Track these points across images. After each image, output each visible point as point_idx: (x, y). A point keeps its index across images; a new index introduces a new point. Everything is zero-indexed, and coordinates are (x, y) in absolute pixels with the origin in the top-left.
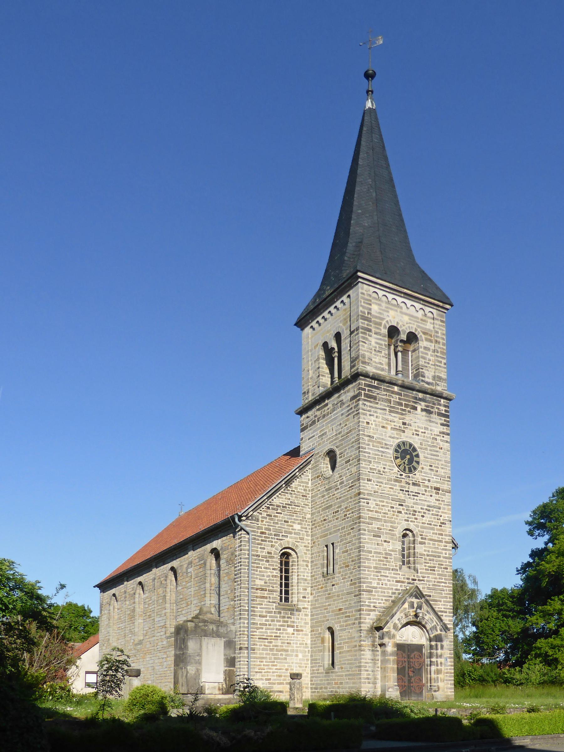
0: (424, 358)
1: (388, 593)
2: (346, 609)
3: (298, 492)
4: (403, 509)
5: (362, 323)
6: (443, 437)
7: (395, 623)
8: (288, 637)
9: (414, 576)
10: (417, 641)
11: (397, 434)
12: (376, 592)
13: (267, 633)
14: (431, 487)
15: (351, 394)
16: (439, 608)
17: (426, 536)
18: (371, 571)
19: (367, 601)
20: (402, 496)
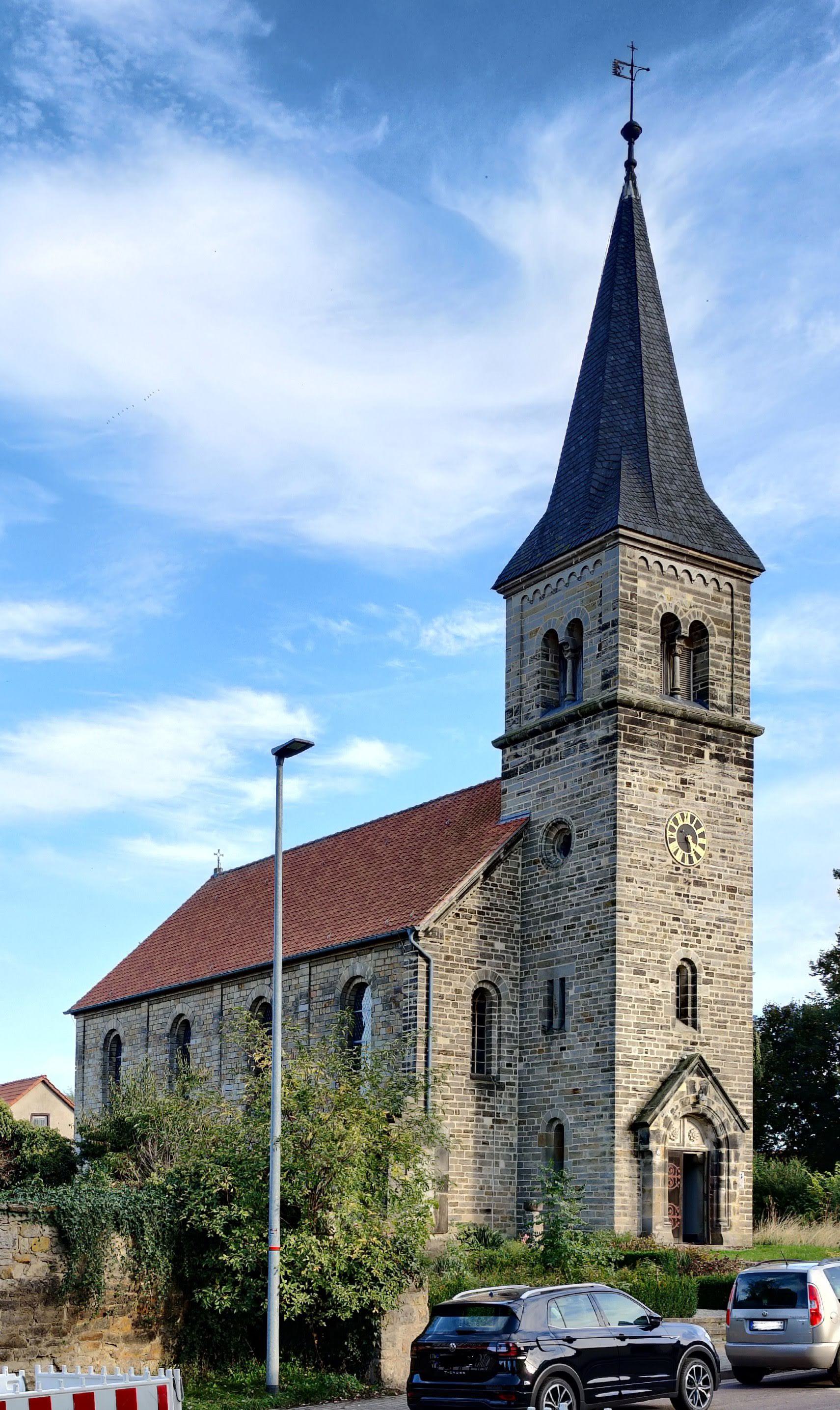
0: (716, 665)
2: (586, 1090)
3: (502, 886)
4: (680, 926)
5: (622, 614)
6: (743, 800)
8: (484, 1132)
9: (694, 1037)
11: (672, 800)
13: (453, 1125)
14: (723, 887)
15: (600, 733)
16: (731, 1090)
17: (714, 970)
19: (624, 1080)
20: (678, 904)
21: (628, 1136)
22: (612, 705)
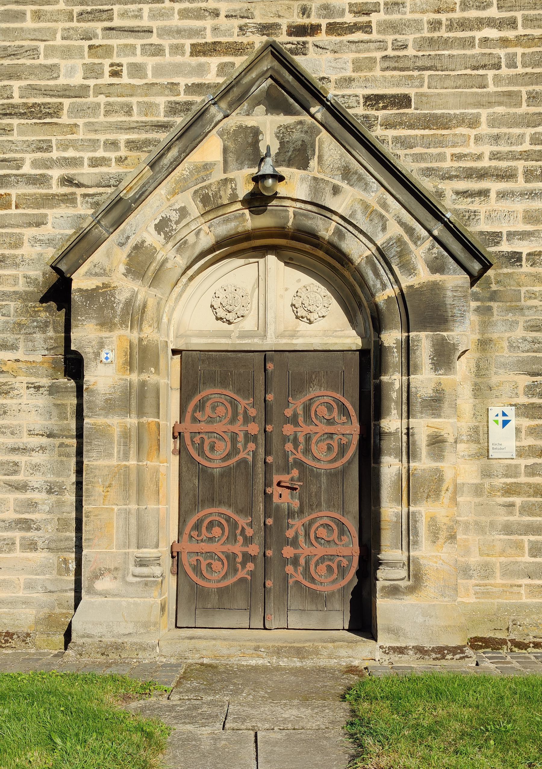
1: (148, 108)
10: (326, 333)
12: (76, 111)
18: (54, 18)
19: (29, 157)
21: (43, 315)
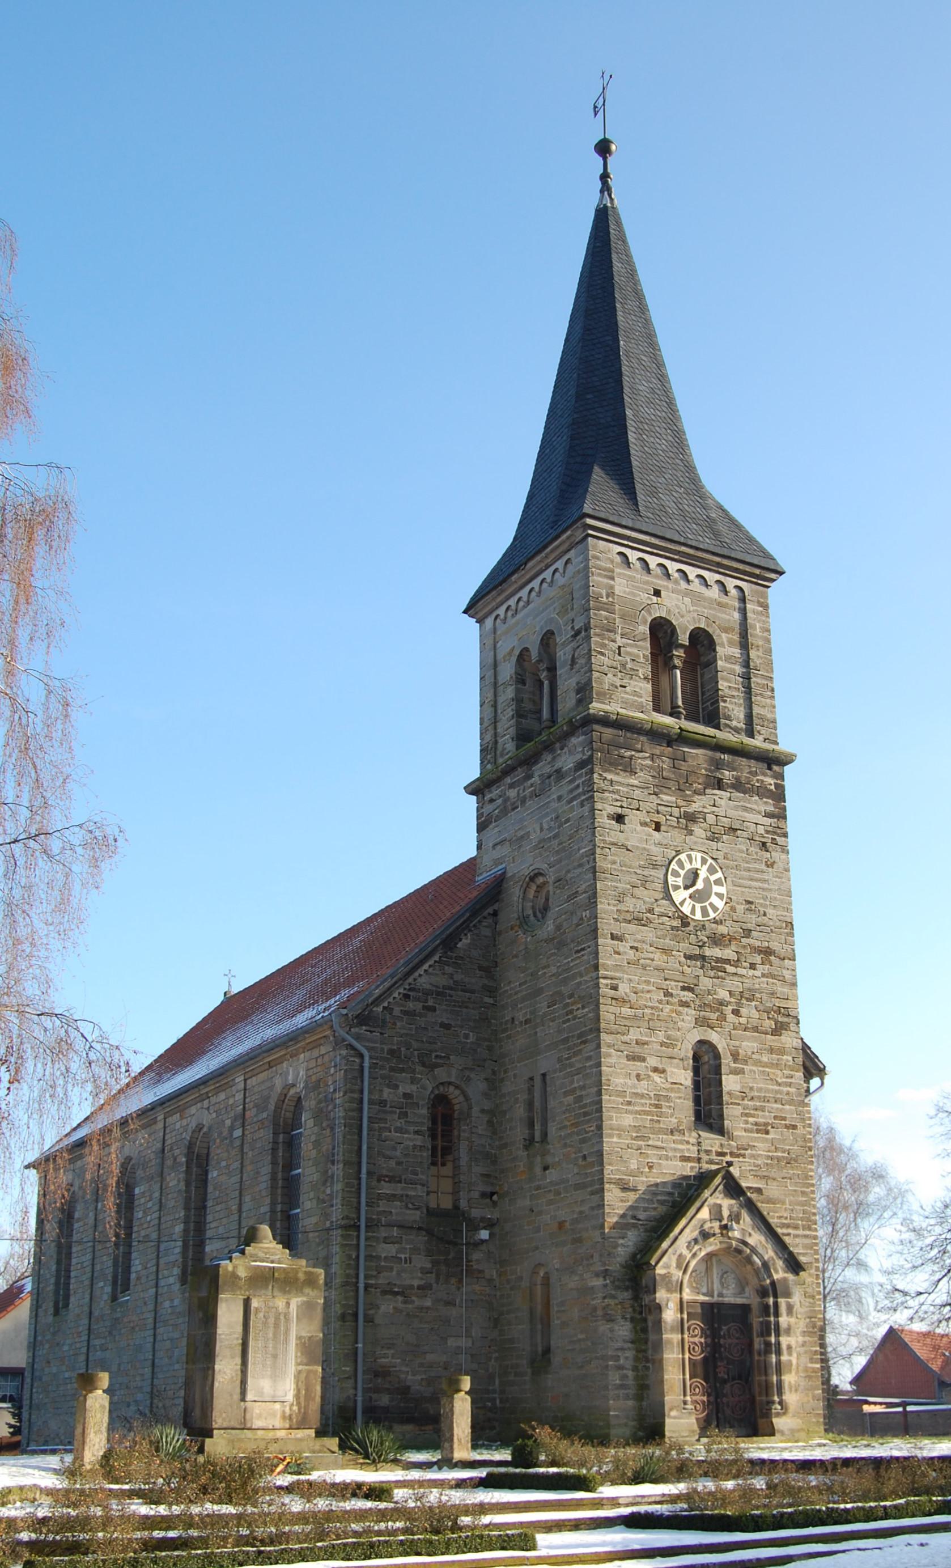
7: (680, 1255)
20: (692, 970)
22: (590, 721)
